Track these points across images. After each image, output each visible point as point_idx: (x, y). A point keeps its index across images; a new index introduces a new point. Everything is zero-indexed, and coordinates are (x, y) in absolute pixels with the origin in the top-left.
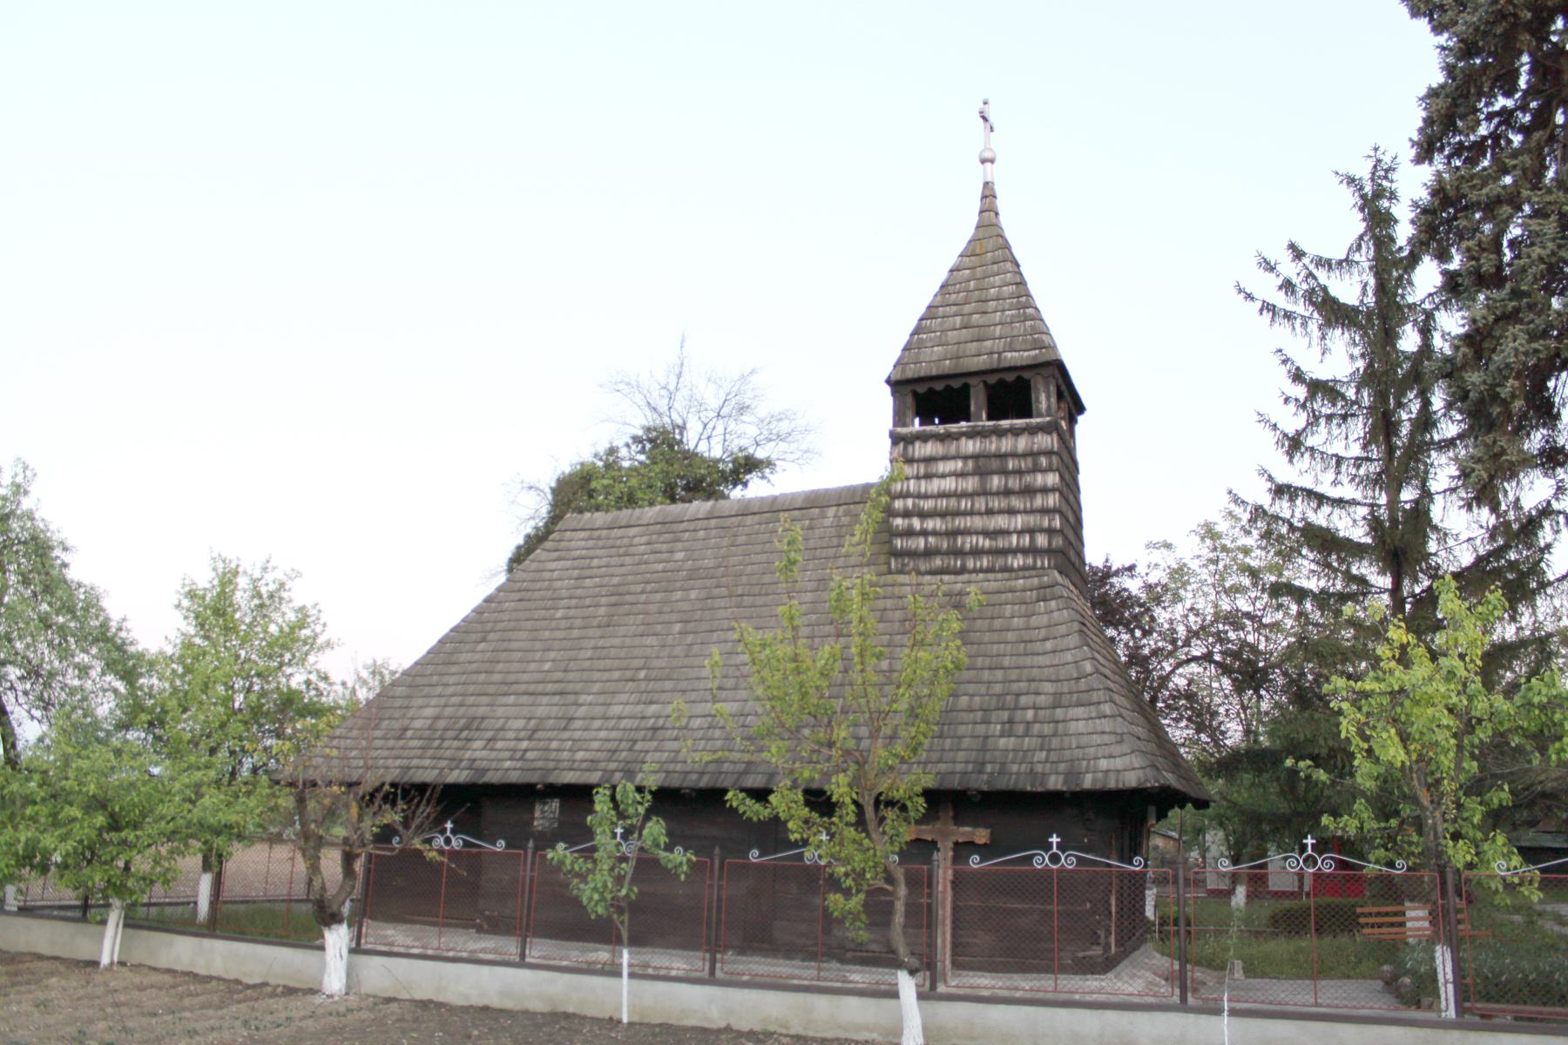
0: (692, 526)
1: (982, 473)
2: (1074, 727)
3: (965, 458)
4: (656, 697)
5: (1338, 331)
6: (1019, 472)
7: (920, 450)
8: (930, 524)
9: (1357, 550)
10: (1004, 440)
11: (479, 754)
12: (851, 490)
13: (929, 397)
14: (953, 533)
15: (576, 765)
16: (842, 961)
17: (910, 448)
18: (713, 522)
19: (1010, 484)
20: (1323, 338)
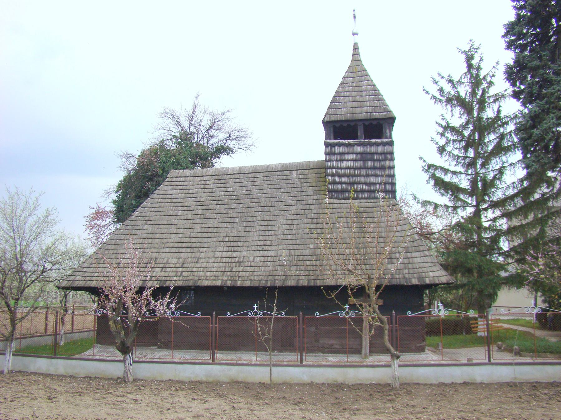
0: (233, 177)
1: (364, 160)
2: (416, 260)
3: (357, 154)
4: (236, 249)
5: (459, 108)
6: (379, 160)
7: (338, 150)
8: (343, 179)
9: (463, 191)
10: (373, 147)
11: (159, 274)
12: (301, 164)
13: (339, 129)
14: (352, 184)
15: (208, 278)
16: (324, 352)
17: (333, 149)
18: (242, 176)
19: (376, 164)
20: (452, 111)
